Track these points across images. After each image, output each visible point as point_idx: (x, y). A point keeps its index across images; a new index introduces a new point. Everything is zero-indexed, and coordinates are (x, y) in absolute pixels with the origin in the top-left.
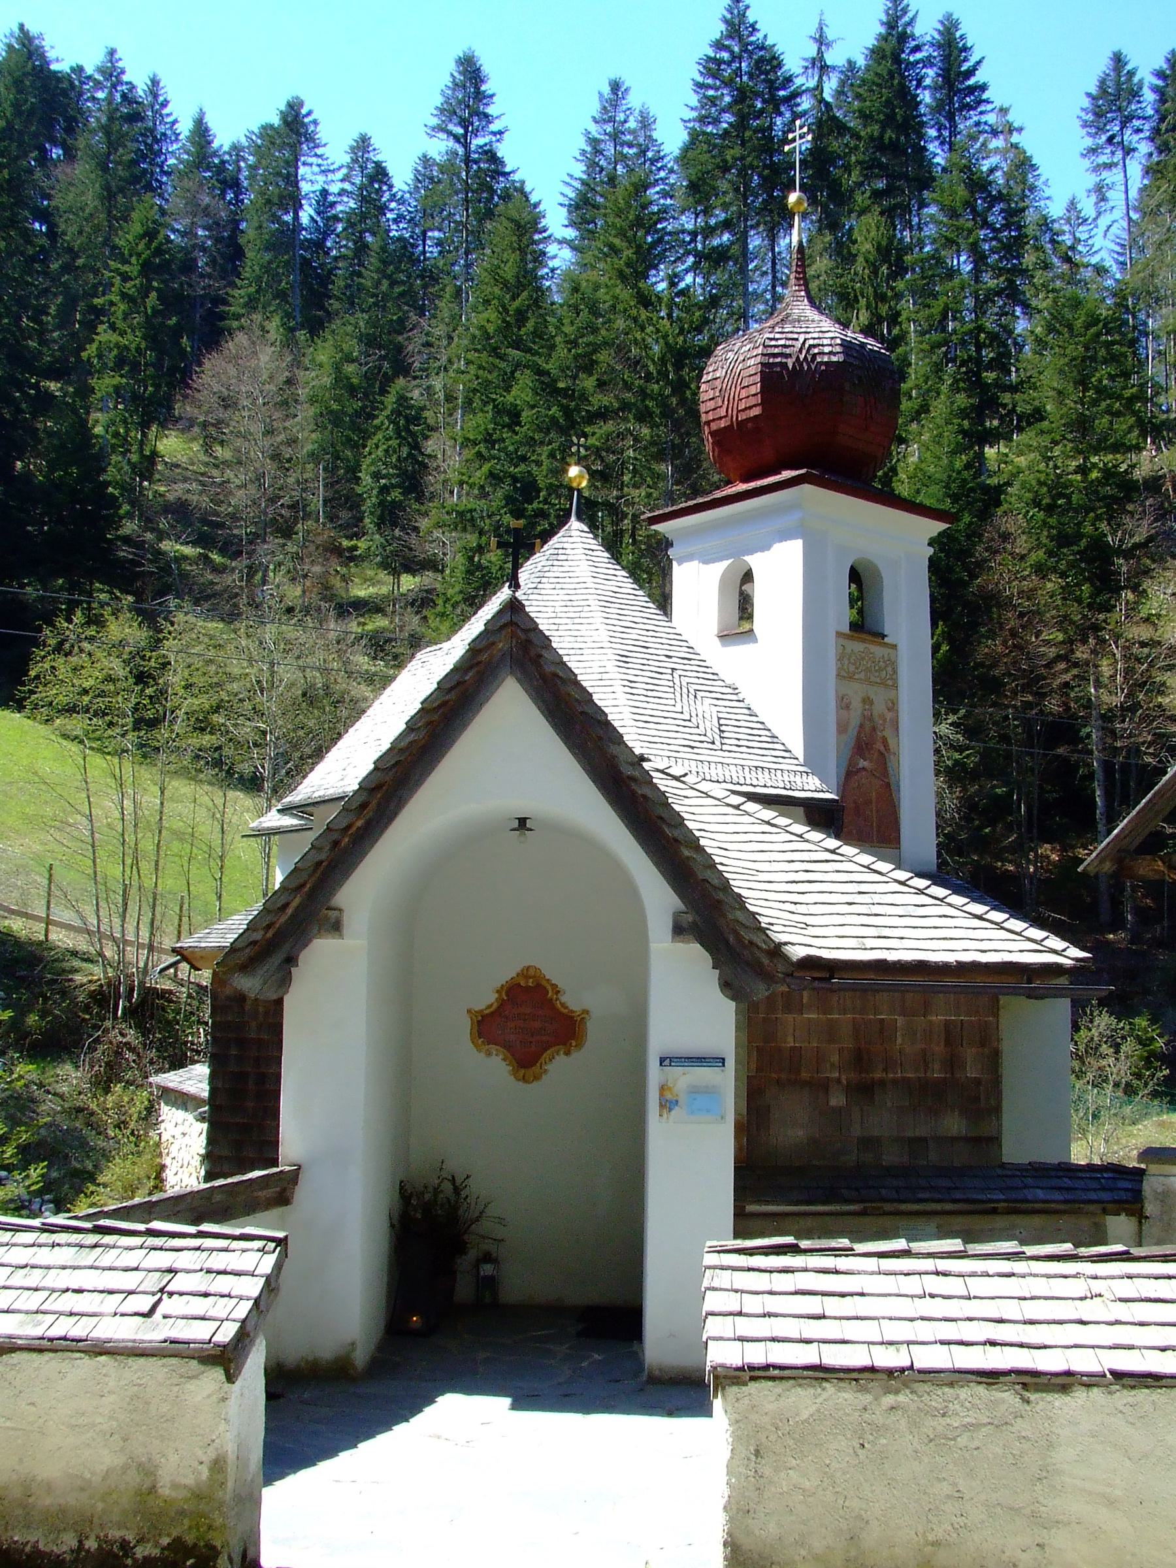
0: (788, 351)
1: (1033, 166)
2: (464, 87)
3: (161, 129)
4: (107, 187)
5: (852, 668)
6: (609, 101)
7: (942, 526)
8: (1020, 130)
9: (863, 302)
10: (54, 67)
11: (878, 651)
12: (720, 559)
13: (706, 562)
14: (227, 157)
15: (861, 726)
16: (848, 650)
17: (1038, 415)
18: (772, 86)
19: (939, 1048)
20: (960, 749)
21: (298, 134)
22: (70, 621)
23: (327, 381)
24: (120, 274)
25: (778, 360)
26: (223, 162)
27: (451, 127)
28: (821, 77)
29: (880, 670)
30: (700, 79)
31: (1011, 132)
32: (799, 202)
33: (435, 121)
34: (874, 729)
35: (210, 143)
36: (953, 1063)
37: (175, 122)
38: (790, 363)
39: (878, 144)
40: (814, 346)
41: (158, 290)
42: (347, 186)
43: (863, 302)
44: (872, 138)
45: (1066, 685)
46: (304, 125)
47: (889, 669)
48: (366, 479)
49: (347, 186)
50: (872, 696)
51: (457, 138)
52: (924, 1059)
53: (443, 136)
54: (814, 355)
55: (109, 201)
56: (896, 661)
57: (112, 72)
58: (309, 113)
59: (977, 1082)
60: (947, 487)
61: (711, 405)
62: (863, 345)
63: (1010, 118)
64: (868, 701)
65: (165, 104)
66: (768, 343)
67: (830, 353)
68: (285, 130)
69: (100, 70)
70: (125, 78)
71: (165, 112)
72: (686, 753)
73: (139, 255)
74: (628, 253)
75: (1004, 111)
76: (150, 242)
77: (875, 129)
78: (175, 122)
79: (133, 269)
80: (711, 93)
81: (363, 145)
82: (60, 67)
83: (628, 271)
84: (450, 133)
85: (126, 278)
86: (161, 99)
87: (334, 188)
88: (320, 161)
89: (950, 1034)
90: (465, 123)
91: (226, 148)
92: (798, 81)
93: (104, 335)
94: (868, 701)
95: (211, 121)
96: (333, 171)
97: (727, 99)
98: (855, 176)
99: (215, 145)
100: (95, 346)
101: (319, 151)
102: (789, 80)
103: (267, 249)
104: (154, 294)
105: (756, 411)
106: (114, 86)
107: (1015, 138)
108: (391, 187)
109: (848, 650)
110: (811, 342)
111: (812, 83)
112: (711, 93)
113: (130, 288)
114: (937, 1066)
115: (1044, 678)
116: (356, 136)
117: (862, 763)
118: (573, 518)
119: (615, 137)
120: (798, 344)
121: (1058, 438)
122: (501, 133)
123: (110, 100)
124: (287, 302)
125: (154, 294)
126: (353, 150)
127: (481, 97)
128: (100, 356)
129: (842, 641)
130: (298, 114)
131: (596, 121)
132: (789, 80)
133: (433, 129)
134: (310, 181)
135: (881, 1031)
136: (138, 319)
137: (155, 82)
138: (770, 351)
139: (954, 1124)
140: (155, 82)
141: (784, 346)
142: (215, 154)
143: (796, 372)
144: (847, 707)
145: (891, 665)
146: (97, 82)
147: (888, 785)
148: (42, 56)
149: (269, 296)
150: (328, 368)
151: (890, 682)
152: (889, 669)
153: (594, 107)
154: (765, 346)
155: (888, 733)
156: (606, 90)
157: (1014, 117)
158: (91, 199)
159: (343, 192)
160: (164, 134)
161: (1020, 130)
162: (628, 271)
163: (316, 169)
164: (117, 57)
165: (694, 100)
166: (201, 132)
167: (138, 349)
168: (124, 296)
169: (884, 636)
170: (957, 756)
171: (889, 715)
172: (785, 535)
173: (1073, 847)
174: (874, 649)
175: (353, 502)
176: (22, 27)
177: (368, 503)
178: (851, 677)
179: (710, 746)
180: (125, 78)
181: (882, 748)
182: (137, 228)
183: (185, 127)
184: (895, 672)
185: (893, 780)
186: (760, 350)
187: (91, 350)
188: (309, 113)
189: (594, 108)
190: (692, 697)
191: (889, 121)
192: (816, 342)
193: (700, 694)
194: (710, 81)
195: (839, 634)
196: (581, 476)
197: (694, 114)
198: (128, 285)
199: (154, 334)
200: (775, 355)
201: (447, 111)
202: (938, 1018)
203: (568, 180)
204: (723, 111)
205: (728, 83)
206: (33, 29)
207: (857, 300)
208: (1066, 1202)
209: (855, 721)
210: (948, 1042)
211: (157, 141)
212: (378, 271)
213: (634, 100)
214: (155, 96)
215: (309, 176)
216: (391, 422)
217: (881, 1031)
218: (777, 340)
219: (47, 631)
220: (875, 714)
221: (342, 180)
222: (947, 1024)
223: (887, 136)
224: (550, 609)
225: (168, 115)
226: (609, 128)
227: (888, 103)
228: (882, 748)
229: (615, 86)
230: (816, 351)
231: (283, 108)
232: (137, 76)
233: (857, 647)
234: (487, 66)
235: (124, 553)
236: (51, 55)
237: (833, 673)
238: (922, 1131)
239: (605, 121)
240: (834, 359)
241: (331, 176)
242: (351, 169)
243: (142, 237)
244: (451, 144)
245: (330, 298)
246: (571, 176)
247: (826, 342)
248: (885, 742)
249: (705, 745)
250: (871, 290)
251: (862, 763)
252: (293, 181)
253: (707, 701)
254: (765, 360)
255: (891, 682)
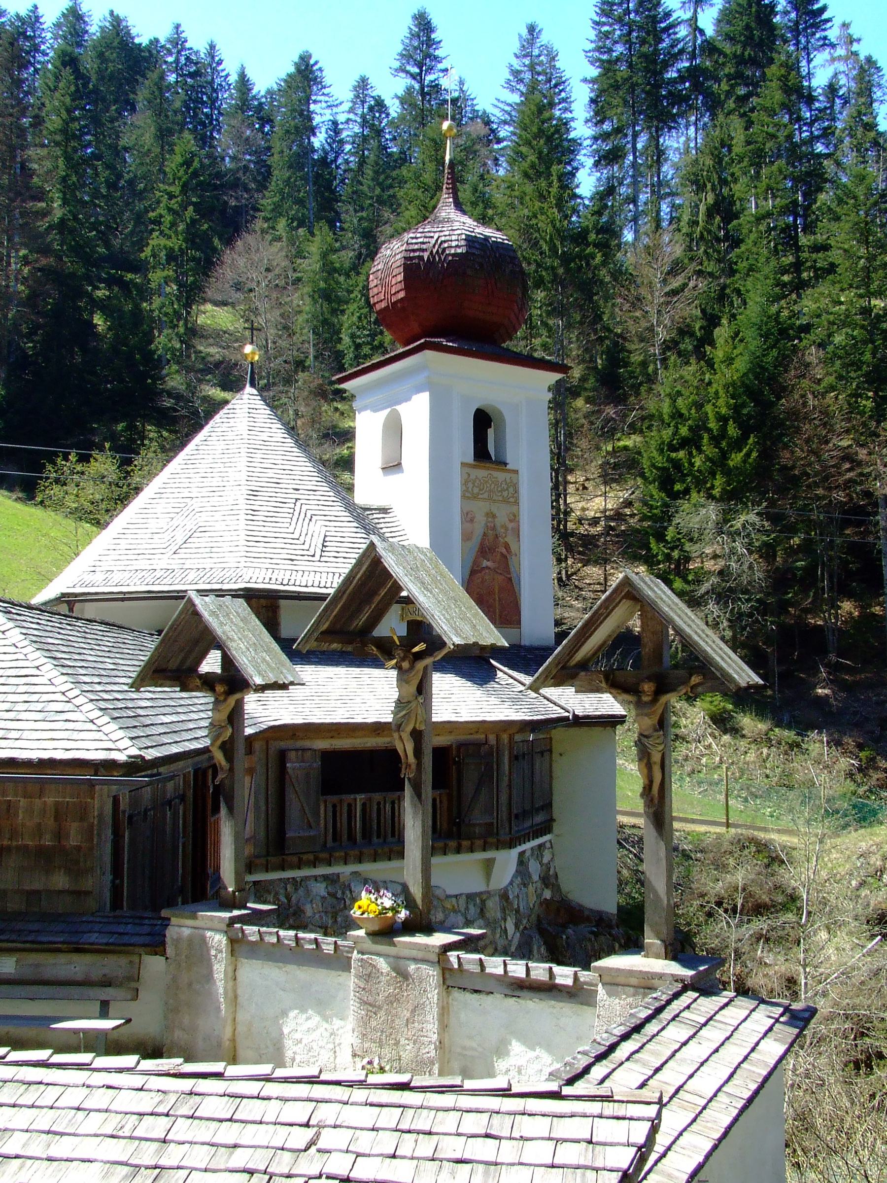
0: (424, 247)
1: (878, 68)
2: (419, 37)
3: (218, 81)
4: (160, 129)
5: (476, 490)
6: (527, 41)
7: (558, 376)
8: (858, 41)
9: (709, 186)
10: (137, 41)
11: (500, 476)
12: (385, 408)
13: (375, 411)
14: (264, 100)
15: (485, 534)
16: (473, 477)
17: (832, 268)
18: (654, 20)
19: (50, 822)
20: (767, 533)
21: (309, 80)
22: (67, 460)
23: (317, 267)
24: (168, 194)
25: (417, 254)
26: (261, 104)
27: (409, 68)
28: (695, 11)
29: (503, 490)
30: (597, 19)
31: (851, 43)
32: (450, 128)
33: (397, 64)
34: (497, 536)
35: (250, 90)
36: (59, 834)
37: (227, 76)
38: (426, 255)
39: (740, 60)
40: (445, 242)
41: (194, 204)
42: (352, 116)
43: (709, 186)
44: (735, 56)
45: (850, 480)
46: (312, 72)
47: (511, 490)
48: (346, 340)
49: (352, 116)
50: (495, 511)
51: (413, 77)
52: (39, 830)
53: (403, 75)
54: (444, 250)
55: (162, 139)
56: (517, 483)
57: (178, 41)
58: (316, 63)
59: (78, 848)
60: (760, 328)
61: (375, 291)
62: (487, 238)
63: (850, 31)
64: (491, 515)
65: (220, 63)
66: (410, 241)
67: (457, 246)
68: (299, 78)
69: (169, 41)
70: (187, 45)
71: (220, 68)
72: (288, 565)
73: (180, 179)
74: (533, 158)
75: (845, 26)
76: (188, 168)
77: (739, 49)
78: (227, 76)
79: (176, 189)
80: (606, 28)
81: (363, 84)
82: (143, 40)
83: (531, 172)
84: (407, 72)
85: (171, 196)
86: (217, 59)
87: (341, 118)
88: (327, 99)
89: (59, 813)
90: (420, 65)
91: (263, 93)
92: (675, 16)
93: (156, 241)
94: (491, 515)
95: (250, 74)
96: (337, 106)
97: (618, 33)
98: (725, 87)
99: (254, 92)
100: (150, 248)
101: (326, 91)
102: (668, 15)
103: (290, 167)
104: (191, 208)
105: (402, 295)
106: (179, 52)
107: (855, 47)
108: (388, 115)
109: (473, 477)
110: (443, 239)
111: (688, 15)
112: (606, 28)
113: (174, 204)
114: (48, 837)
115: (834, 476)
116: (357, 78)
117: (485, 563)
118: (248, 385)
119: (532, 68)
120: (433, 241)
121: (846, 286)
122: (446, 70)
123: (177, 61)
124: (305, 207)
125: (191, 208)
126: (355, 88)
127: (431, 43)
128: (154, 255)
129: (468, 470)
130: (307, 65)
131: (517, 57)
132: (668, 15)
133: (396, 70)
134: (321, 115)
135: (8, 810)
136: (181, 227)
137: (212, 47)
138: (411, 247)
139: (60, 881)
140: (212, 47)
141: (423, 243)
142: (254, 98)
143: (431, 263)
144: (472, 521)
145: (515, 487)
146: (169, 50)
147: (510, 579)
148: (128, 33)
149: (289, 203)
150: (317, 257)
151: (512, 500)
152: (511, 490)
153: (515, 46)
154: (408, 244)
155: (510, 539)
156: (524, 32)
157: (854, 31)
158: (148, 138)
159: (348, 121)
160: (221, 85)
161: (858, 41)
162: (531, 172)
163: (324, 105)
164: (181, 29)
165: (592, 35)
166: (244, 82)
167: (180, 249)
168: (170, 210)
169: (506, 464)
170: (765, 538)
171: (510, 526)
172: (419, 390)
173: (870, 606)
174: (496, 474)
175: (339, 356)
176: (112, 13)
177: (347, 358)
178: (475, 497)
179: (310, 558)
180: (187, 45)
181: (504, 551)
182: (179, 159)
183: (233, 79)
184: (516, 491)
185: (514, 575)
186: (404, 248)
187: (148, 251)
188: (316, 63)
189: (516, 47)
190: (307, 520)
191: (749, 41)
192: (448, 238)
193: (314, 518)
194: (604, 19)
195: (463, 465)
196: (253, 353)
197: (593, 45)
198: (173, 202)
199: (193, 238)
200: (414, 251)
201: (406, 56)
202: (50, 800)
203: (496, 103)
204: (616, 42)
205: (620, 20)
206: (120, 12)
207: (705, 186)
208: (107, 944)
209: (479, 529)
210: (56, 818)
211: (215, 91)
212: (373, 179)
213: (544, 39)
214: (213, 57)
215: (318, 111)
216: (363, 295)
217: (8, 810)
218: (416, 238)
219: (49, 467)
220: (498, 524)
221: (349, 112)
222: (57, 804)
223: (746, 53)
224: (211, 456)
225: (223, 70)
226: (527, 61)
227: (747, 27)
228: (504, 551)
229: (532, 29)
230: (446, 245)
231: (296, 59)
232: (197, 43)
233: (481, 473)
234: (436, 20)
235: (168, 403)
236: (134, 32)
237: (458, 493)
238: (37, 885)
239: (525, 56)
240: (459, 251)
241: (335, 110)
242: (355, 103)
243: (182, 165)
244: (409, 81)
245: (338, 201)
246: (498, 100)
247: (454, 238)
248: (507, 546)
249: (306, 558)
250: (715, 176)
251: (485, 563)
252: (308, 117)
253: (319, 523)
254: (407, 255)
255: (512, 496)
